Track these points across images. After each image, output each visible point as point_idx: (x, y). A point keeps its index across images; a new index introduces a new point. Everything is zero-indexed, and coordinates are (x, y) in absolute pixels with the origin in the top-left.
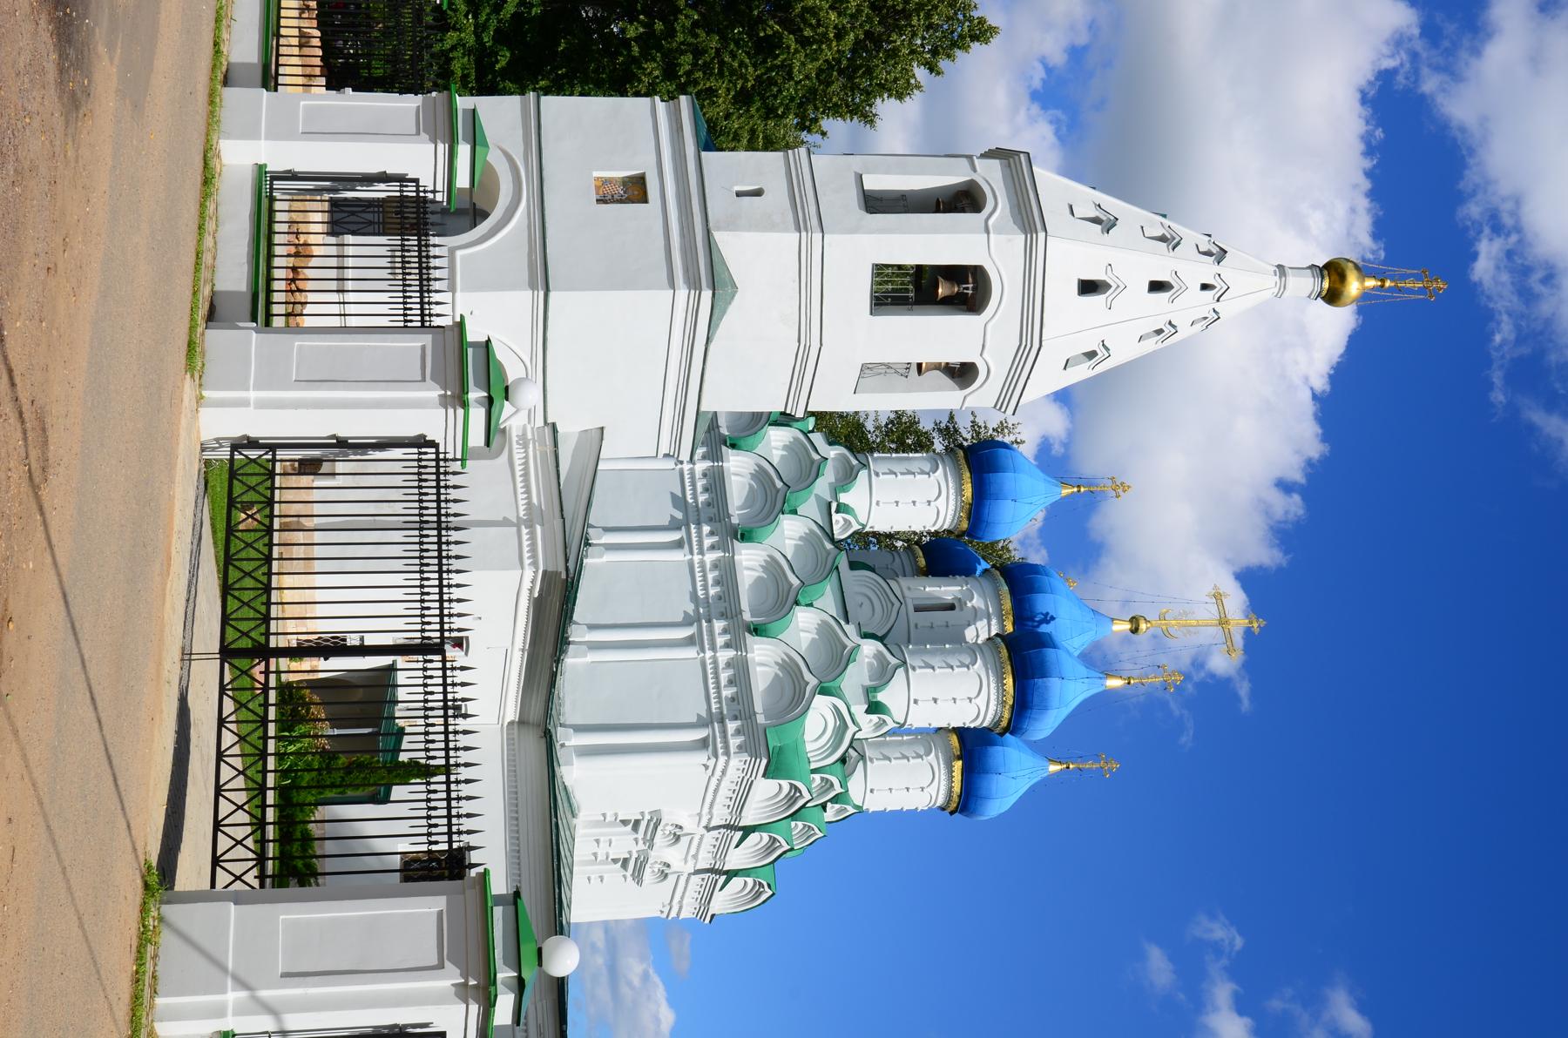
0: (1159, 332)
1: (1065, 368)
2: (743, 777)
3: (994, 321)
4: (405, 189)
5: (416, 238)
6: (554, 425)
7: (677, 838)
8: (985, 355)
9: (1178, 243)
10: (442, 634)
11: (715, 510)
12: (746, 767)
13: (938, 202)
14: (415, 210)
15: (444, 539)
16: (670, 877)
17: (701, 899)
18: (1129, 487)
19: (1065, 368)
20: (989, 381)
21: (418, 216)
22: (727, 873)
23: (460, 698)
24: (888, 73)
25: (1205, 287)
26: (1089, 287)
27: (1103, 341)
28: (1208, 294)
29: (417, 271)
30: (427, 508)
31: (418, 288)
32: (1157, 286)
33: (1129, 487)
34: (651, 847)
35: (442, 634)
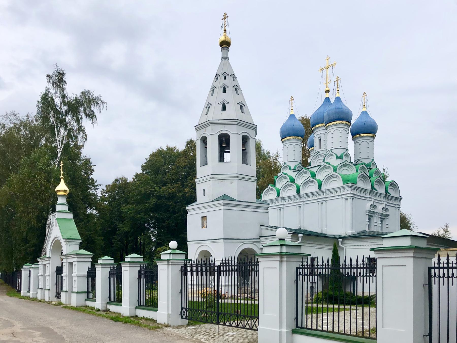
0: (236, 89)
1: (244, 113)
2: (356, 189)
3: (231, 132)
4: (301, 273)
5: (249, 266)
6: (260, 237)
7: (375, 206)
8: (240, 133)
9: (215, 86)
10: (365, 268)
11: (293, 199)
12: (353, 189)
13: (205, 148)
14: (254, 266)
15: (349, 267)
16: (387, 207)
17: (395, 199)
18: (364, 92)
19: (244, 113)
20: (247, 132)
21: (250, 265)
22: (386, 193)
23: (362, 262)
24: (47, 156)
25: (225, 78)
26: (224, 108)
27: (237, 104)
28: (227, 77)
29: (304, 270)
30: (360, 273)
31: (306, 270)
32: (224, 91)
33: (364, 92)
34: (377, 212)
35: (365, 268)
